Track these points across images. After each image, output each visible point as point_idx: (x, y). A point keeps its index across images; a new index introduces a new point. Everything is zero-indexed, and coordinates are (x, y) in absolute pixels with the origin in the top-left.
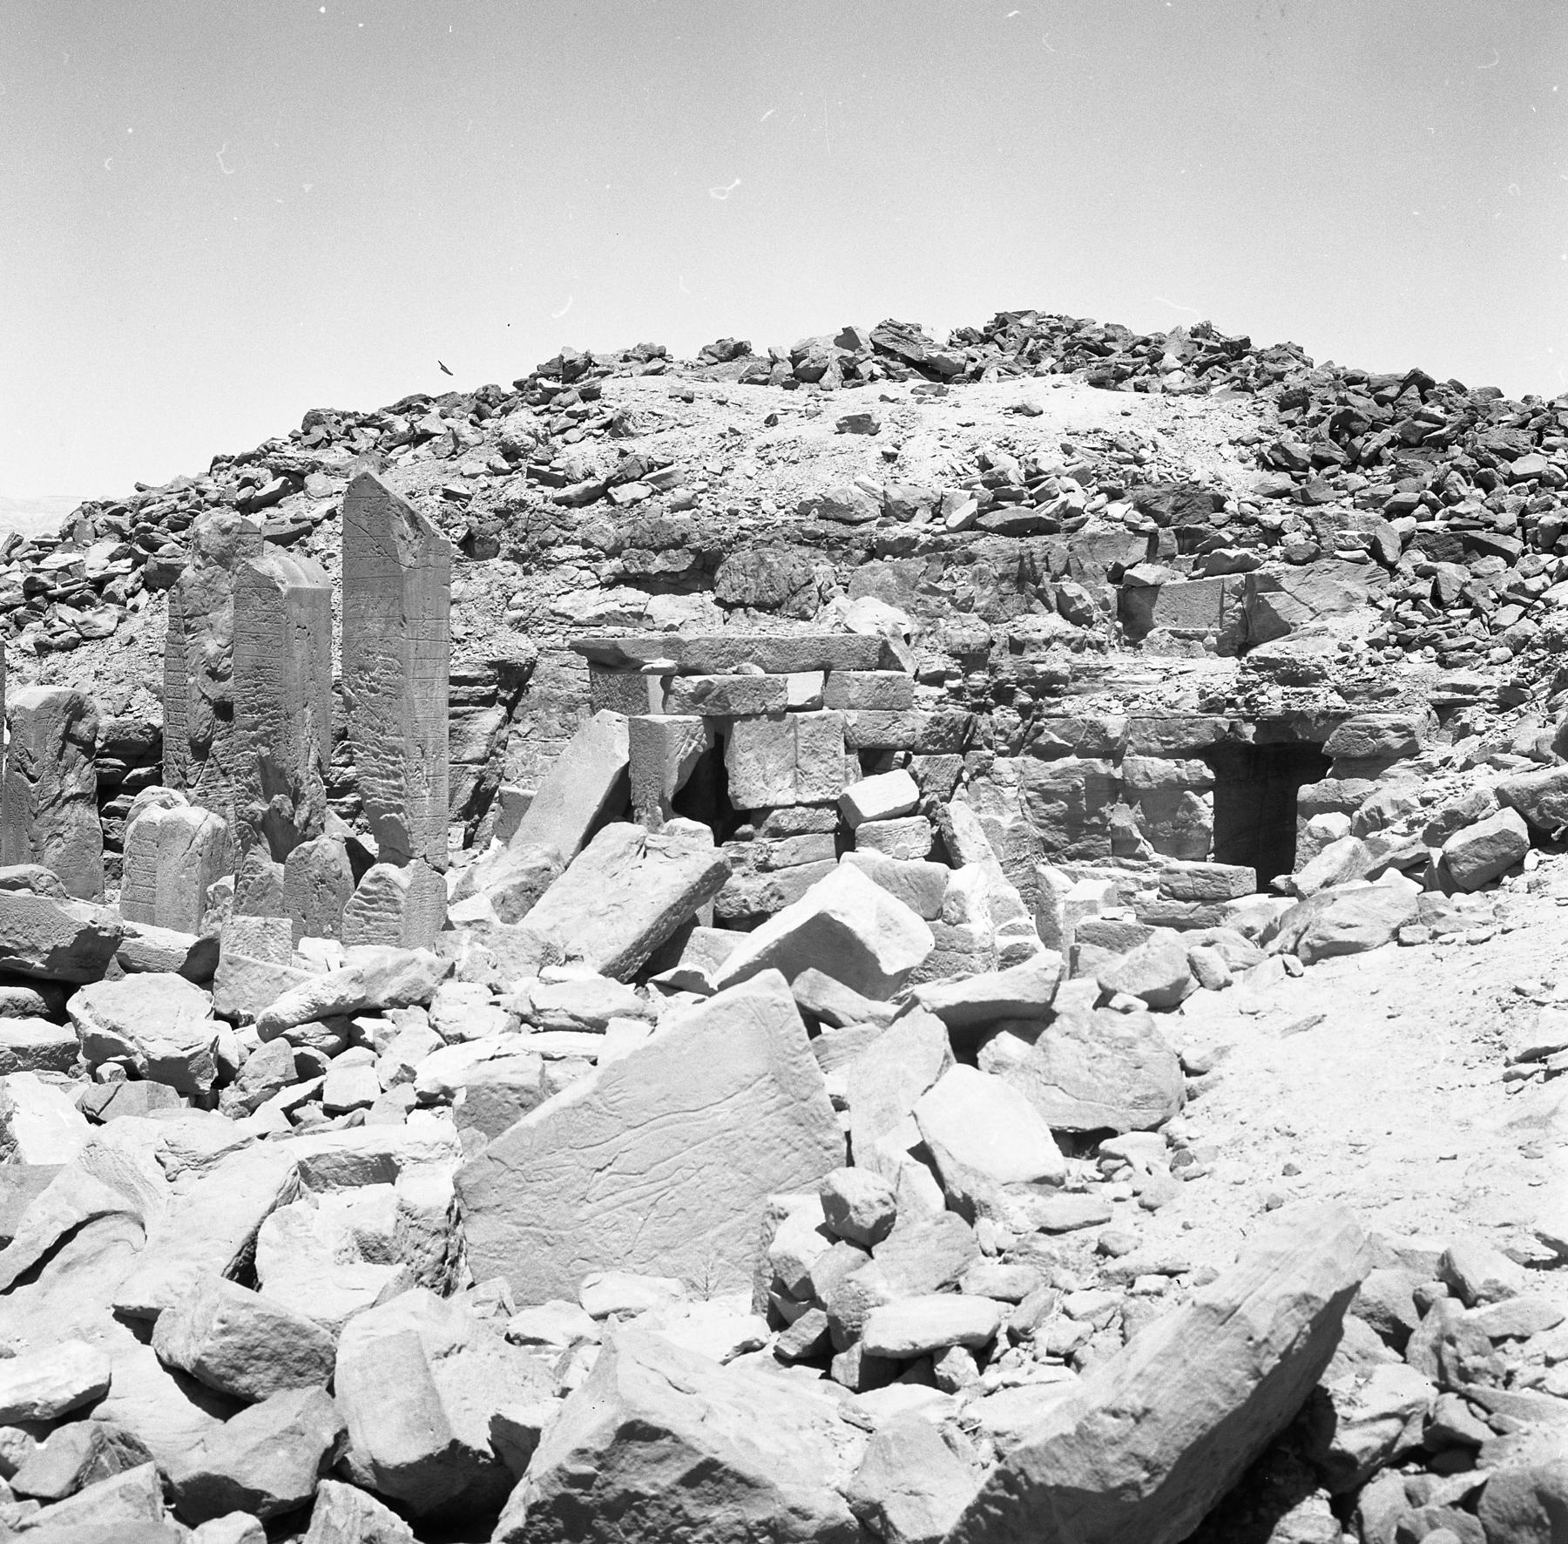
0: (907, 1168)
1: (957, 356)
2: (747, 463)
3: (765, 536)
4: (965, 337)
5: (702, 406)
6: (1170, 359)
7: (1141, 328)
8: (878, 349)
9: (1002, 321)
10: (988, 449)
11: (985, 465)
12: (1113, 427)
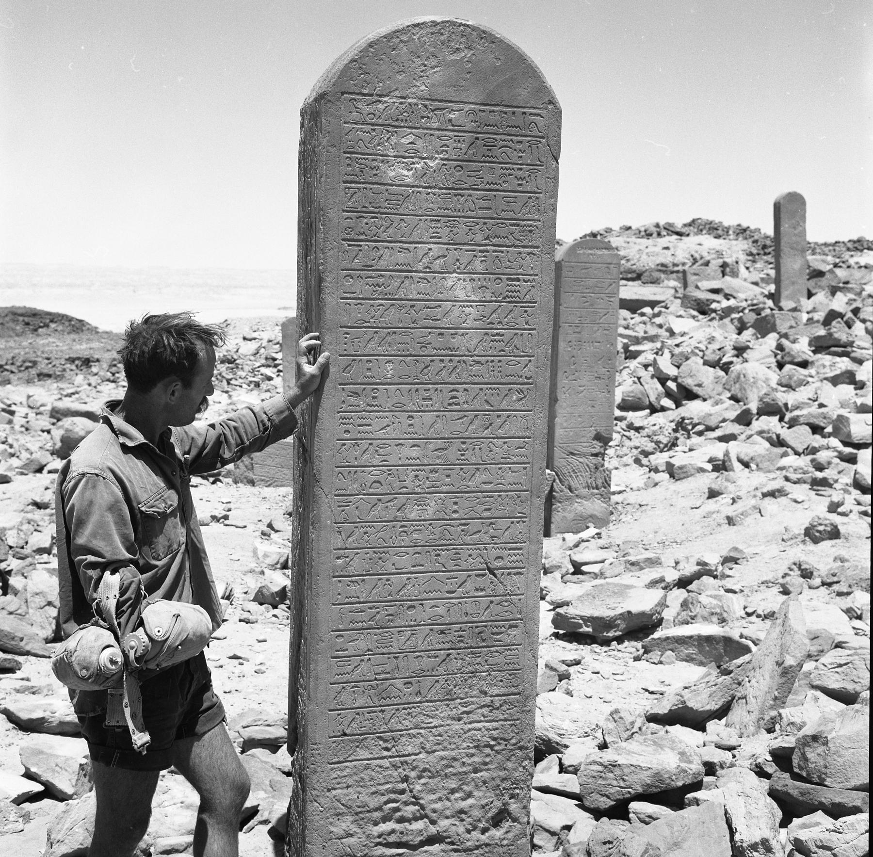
0: (672, 461)
1: (683, 230)
2: (644, 257)
3: (651, 270)
4: (685, 225)
5: (631, 244)
6: (731, 232)
7: (726, 224)
8: (665, 228)
9: (694, 221)
10: (693, 253)
11: (692, 256)
12: (718, 248)
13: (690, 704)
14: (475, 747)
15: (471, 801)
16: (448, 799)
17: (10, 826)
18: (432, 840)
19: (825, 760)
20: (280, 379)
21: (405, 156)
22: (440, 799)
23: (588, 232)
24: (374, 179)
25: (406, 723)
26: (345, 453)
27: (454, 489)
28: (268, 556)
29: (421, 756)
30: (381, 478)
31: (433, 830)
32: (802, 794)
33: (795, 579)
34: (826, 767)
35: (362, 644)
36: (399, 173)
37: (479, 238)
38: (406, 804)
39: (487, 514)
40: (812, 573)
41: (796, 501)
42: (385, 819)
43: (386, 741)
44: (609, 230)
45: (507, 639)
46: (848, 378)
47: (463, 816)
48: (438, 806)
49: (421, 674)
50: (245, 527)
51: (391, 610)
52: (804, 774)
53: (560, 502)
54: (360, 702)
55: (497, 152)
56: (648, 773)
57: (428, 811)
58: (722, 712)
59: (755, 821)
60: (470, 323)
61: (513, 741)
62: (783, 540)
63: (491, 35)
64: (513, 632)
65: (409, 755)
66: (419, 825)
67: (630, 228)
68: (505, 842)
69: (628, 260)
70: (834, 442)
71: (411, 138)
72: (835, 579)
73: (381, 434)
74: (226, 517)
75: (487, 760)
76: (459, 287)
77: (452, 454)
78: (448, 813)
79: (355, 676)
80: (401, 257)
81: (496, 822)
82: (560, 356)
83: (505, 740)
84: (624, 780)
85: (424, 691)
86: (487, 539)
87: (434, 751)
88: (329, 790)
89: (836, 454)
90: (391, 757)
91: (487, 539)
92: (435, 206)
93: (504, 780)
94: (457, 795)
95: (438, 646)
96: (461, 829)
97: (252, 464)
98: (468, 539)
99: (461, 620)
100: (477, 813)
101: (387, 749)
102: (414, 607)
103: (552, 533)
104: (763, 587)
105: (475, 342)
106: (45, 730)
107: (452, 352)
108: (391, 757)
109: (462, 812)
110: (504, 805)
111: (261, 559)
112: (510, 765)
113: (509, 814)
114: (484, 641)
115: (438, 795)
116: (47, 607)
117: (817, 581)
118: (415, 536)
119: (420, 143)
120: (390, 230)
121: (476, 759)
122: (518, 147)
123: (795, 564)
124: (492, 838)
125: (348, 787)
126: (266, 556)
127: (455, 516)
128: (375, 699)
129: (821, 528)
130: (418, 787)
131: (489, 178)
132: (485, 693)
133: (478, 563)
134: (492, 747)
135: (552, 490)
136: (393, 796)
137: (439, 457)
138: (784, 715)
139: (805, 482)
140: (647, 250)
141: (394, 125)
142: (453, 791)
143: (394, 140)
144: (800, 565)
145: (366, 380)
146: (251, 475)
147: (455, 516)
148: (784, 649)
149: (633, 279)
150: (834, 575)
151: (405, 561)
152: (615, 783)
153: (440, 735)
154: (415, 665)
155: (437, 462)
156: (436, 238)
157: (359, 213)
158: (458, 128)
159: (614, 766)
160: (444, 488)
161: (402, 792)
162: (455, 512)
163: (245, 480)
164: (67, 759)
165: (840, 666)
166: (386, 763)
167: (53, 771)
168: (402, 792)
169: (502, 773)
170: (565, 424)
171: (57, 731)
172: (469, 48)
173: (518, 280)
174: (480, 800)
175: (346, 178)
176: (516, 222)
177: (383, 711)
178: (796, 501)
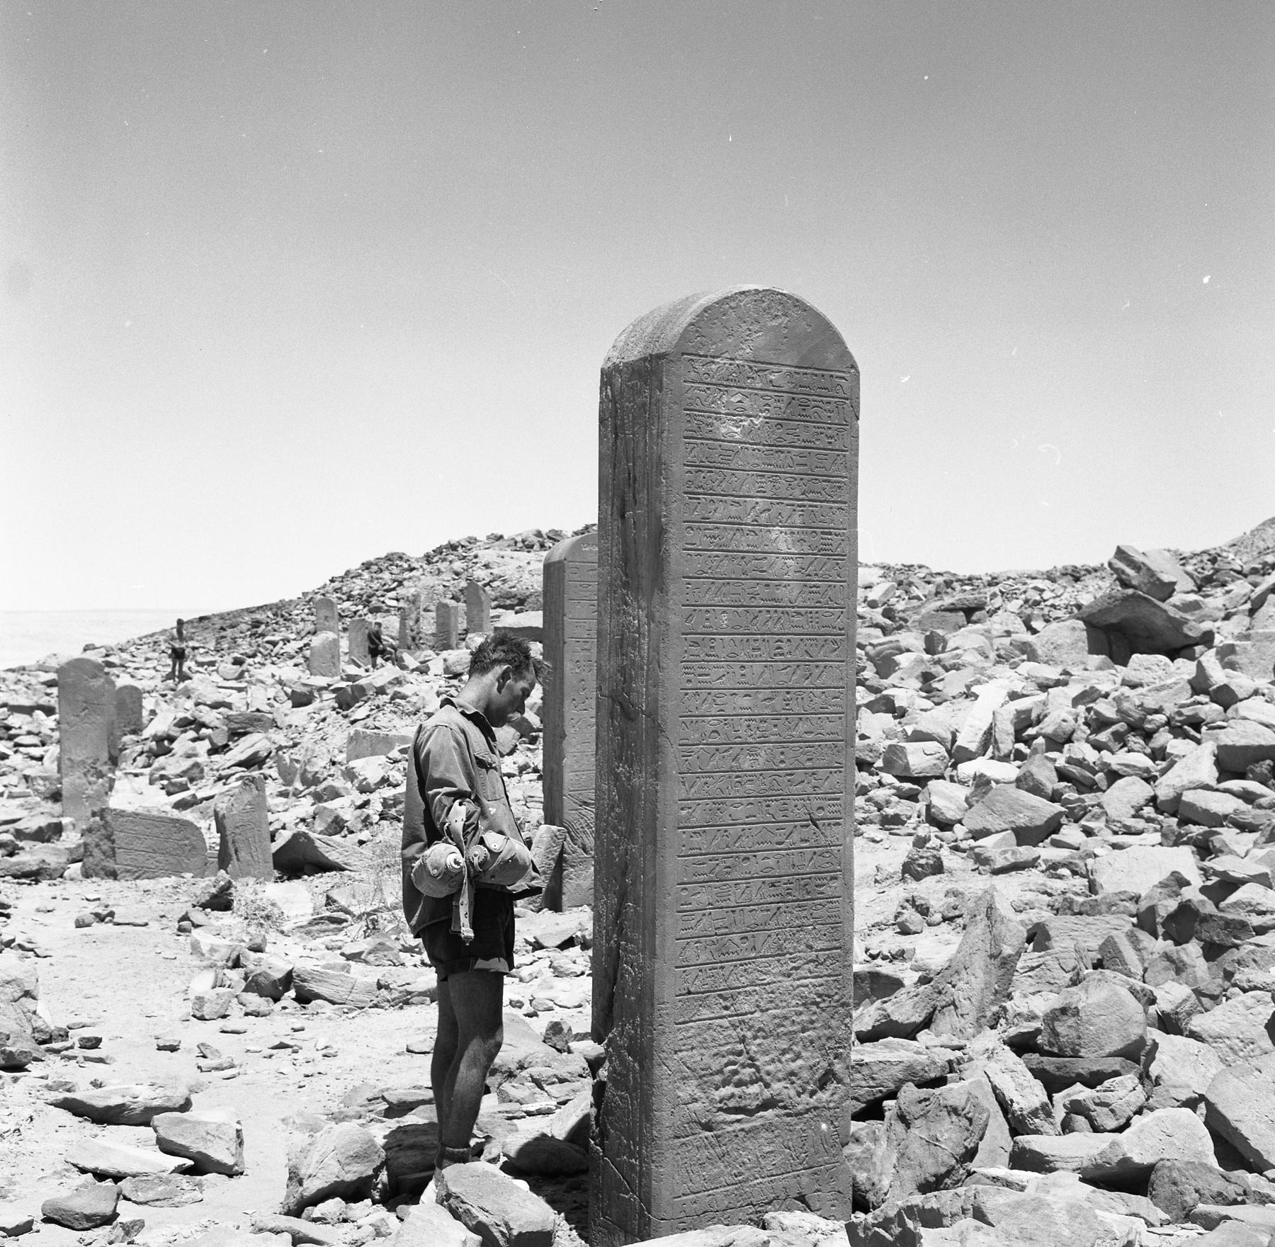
2: (526, 575)
8: (550, 538)
13: (895, 1017)
14: (804, 1004)
15: (800, 1062)
16: (780, 1061)
17: (187, 1196)
18: (767, 1105)
19: (1077, 1030)
20: (19, 756)
21: (736, 413)
22: (773, 1061)
23: (445, 543)
24: (710, 435)
25: (743, 979)
26: (688, 703)
27: (781, 739)
28: (216, 951)
29: (756, 1015)
30: (718, 728)
31: (767, 1094)
32: (1059, 1069)
33: (911, 915)
34: (1079, 1038)
35: (704, 898)
36: (729, 429)
37: (797, 493)
38: (743, 1066)
39: (809, 764)
40: (928, 909)
41: (874, 841)
42: (725, 1083)
43: (725, 999)
44: (472, 541)
45: (829, 892)
46: (884, 705)
47: (793, 1078)
48: (771, 1068)
49: (756, 928)
50: (146, 924)
51: (729, 862)
52: (1056, 1050)
53: (573, 866)
54: (703, 959)
55: (810, 411)
56: (900, 1067)
57: (763, 1074)
58: (927, 1023)
59: (1028, 1090)
60: (791, 575)
61: (836, 997)
62: (876, 881)
63: (803, 303)
64: (834, 884)
65: (746, 1014)
66: (754, 1089)
67: (501, 537)
68: (832, 1105)
69: (504, 581)
70: (888, 778)
71: (739, 397)
72: (957, 913)
73: (717, 684)
74: (112, 914)
75: (814, 1018)
76: (781, 539)
77: (778, 703)
78: (780, 1075)
79: (696, 932)
80: (734, 510)
81: (822, 1085)
82: (566, 680)
83: (829, 996)
84: (873, 1079)
85: (758, 946)
86: (810, 790)
87: (768, 1010)
88: (676, 1052)
89: (893, 791)
90: (730, 1016)
91: (810, 790)
92: (760, 462)
93: (829, 1038)
94: (788, 1056)
95: (769, 900)
96: (792, 1093)
97: (113, 849)
98: (794, 789)
99: (789, 872)
100: (805, 1075)
101: (726, 1008)
102: (747, 859)
103: (564, 908)
104: (875, 930)
105: (796, 592)
106: (124, 1120)
107: (775, 604)
108: (730, 1016)
109: (792, 1073)
110: (830, 1065)
111: (207, 955)
112: (833, 1023)
113: (834, 1075)
114: (808, 893)
115: (772, 1056)
116: (24, 999)
117: (938, 917)
118: (748, 786)
119: (747, 403)
120: (724, 484)
121: (804, 1017)
122: (828, 407)
123: (907, 901)
124: (819, 1100)
125: (693, 1048)
126: (213, 950)
127: (782, 766)
128: (716, 955)
129: (923, 861)
130: (754, 1048)
131: (804, 436)
132: (810, 947)
133: (802, 813)
134: (817, 1004)
135: (562, 852)
136: (732, 1058)
137: (767, 707)
138: (1008, 1007)
139: (872, 822)
140: (530, 567)
141: (725, 385)
142: (784, 1052)
143: (725, 399)
144: (914, 901)
145: (704, 630)
146: (110, 864)
147: (782, 766)
148: (996, 940)
149: (511, 607)
150: (955, 908)
151: (740, 812)
152: (864, 1083)
153: (773, 992)
154: (750, 919)
155: (766, 711)
156: (761, 493)
157: (699, 467)
158: (777, 389)
159: (861, 1065)
160: (773, 738)
161: (740, 1054)
162: (782, 762)
163: (102, 873)
164: (219, 1126)
165: (1032, 969)
166: (725, 1022)
167: (204, 1139)
168: (740, 1054)
169: (826, 1032)
170: (576, 767)
171: (140, 1120)
172: (785, 315)
173: (830, 534)
174: (808, 1061)
175: (686, 433)
176: (828, 478)
177: (722, 968)
178: (874, 841)
